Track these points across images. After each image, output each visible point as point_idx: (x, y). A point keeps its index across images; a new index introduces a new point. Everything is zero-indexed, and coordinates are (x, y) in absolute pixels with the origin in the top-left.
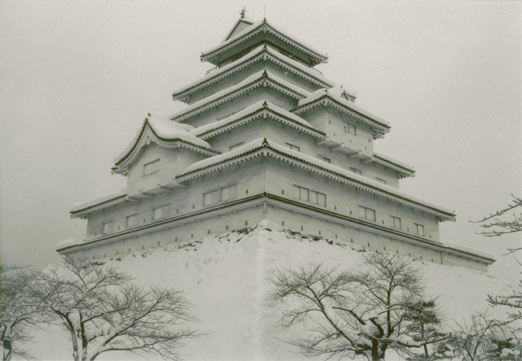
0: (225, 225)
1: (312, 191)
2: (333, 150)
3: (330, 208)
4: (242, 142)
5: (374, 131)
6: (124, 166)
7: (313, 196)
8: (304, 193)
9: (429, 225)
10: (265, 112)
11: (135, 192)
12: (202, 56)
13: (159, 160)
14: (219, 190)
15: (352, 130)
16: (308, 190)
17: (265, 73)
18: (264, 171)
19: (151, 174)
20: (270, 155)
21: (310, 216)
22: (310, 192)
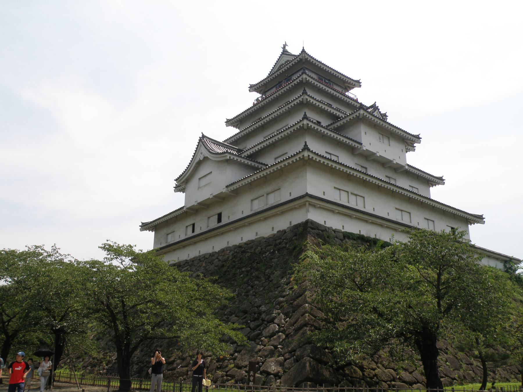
0: (271, 227)
1: (352, 193)
2: (370, 157)
4: (285, 152)
5: (407, 143)
6: (182, 181)
7: (352, 198)
8: (344, 195)
10: (306, 154)
11: (193, 203)
12: (249, 87)
13: (211, 172)
14: (265, 195)
15: (386, 141)
16: (348, 192)
17: (305, 115)
18: (306, 173)
19: (205, 186)
20: (311, 157)
22: (350, 194)
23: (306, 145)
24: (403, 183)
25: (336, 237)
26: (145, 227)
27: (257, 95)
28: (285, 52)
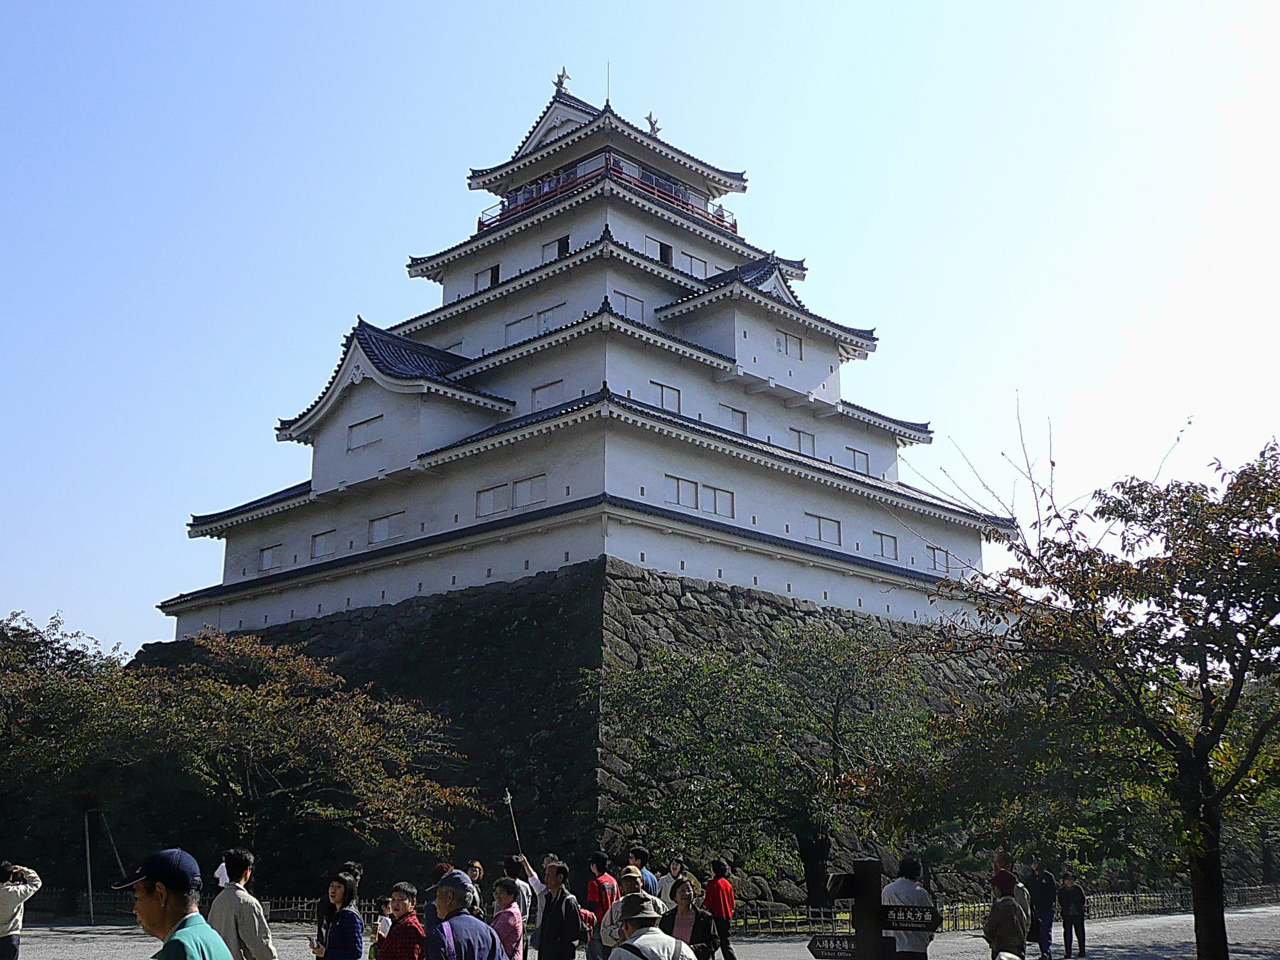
2: (750, 387)
3: (742, 521)
7: (705, 496)
9: (957, 547)
10: (606, 320)
14: (510, 485)
15: (793, 348)
20: (615, 416)
21: (699, 540)
23: (607, 231)
24: (832, 449)
25: (666, 591)
26: (202, 525)
27: (490, 204)
28: (561, 97)
